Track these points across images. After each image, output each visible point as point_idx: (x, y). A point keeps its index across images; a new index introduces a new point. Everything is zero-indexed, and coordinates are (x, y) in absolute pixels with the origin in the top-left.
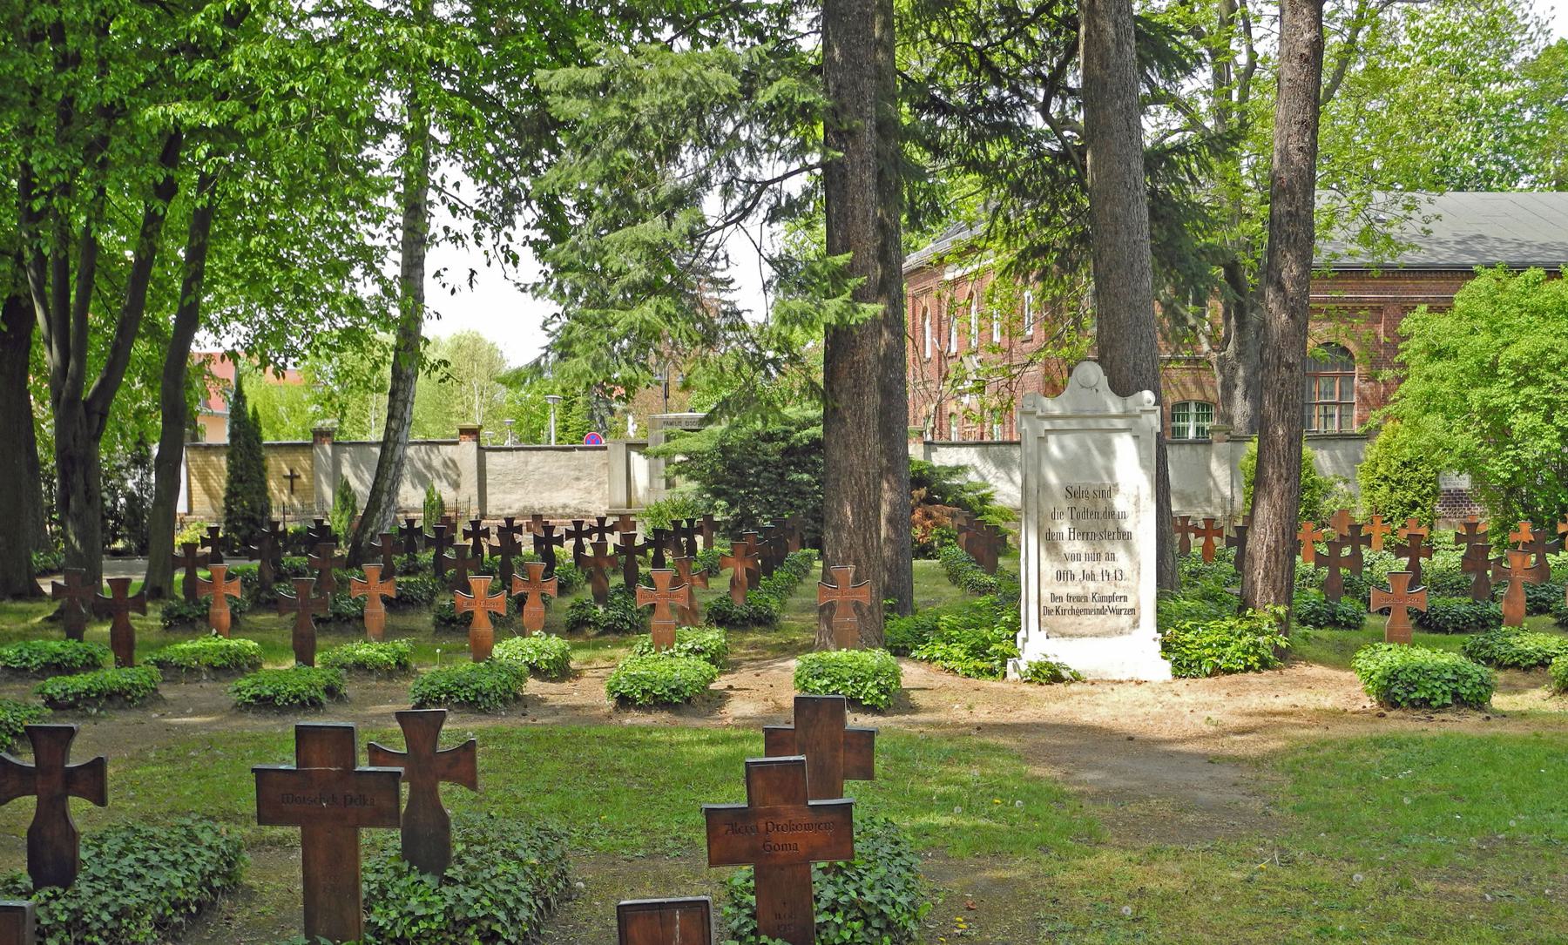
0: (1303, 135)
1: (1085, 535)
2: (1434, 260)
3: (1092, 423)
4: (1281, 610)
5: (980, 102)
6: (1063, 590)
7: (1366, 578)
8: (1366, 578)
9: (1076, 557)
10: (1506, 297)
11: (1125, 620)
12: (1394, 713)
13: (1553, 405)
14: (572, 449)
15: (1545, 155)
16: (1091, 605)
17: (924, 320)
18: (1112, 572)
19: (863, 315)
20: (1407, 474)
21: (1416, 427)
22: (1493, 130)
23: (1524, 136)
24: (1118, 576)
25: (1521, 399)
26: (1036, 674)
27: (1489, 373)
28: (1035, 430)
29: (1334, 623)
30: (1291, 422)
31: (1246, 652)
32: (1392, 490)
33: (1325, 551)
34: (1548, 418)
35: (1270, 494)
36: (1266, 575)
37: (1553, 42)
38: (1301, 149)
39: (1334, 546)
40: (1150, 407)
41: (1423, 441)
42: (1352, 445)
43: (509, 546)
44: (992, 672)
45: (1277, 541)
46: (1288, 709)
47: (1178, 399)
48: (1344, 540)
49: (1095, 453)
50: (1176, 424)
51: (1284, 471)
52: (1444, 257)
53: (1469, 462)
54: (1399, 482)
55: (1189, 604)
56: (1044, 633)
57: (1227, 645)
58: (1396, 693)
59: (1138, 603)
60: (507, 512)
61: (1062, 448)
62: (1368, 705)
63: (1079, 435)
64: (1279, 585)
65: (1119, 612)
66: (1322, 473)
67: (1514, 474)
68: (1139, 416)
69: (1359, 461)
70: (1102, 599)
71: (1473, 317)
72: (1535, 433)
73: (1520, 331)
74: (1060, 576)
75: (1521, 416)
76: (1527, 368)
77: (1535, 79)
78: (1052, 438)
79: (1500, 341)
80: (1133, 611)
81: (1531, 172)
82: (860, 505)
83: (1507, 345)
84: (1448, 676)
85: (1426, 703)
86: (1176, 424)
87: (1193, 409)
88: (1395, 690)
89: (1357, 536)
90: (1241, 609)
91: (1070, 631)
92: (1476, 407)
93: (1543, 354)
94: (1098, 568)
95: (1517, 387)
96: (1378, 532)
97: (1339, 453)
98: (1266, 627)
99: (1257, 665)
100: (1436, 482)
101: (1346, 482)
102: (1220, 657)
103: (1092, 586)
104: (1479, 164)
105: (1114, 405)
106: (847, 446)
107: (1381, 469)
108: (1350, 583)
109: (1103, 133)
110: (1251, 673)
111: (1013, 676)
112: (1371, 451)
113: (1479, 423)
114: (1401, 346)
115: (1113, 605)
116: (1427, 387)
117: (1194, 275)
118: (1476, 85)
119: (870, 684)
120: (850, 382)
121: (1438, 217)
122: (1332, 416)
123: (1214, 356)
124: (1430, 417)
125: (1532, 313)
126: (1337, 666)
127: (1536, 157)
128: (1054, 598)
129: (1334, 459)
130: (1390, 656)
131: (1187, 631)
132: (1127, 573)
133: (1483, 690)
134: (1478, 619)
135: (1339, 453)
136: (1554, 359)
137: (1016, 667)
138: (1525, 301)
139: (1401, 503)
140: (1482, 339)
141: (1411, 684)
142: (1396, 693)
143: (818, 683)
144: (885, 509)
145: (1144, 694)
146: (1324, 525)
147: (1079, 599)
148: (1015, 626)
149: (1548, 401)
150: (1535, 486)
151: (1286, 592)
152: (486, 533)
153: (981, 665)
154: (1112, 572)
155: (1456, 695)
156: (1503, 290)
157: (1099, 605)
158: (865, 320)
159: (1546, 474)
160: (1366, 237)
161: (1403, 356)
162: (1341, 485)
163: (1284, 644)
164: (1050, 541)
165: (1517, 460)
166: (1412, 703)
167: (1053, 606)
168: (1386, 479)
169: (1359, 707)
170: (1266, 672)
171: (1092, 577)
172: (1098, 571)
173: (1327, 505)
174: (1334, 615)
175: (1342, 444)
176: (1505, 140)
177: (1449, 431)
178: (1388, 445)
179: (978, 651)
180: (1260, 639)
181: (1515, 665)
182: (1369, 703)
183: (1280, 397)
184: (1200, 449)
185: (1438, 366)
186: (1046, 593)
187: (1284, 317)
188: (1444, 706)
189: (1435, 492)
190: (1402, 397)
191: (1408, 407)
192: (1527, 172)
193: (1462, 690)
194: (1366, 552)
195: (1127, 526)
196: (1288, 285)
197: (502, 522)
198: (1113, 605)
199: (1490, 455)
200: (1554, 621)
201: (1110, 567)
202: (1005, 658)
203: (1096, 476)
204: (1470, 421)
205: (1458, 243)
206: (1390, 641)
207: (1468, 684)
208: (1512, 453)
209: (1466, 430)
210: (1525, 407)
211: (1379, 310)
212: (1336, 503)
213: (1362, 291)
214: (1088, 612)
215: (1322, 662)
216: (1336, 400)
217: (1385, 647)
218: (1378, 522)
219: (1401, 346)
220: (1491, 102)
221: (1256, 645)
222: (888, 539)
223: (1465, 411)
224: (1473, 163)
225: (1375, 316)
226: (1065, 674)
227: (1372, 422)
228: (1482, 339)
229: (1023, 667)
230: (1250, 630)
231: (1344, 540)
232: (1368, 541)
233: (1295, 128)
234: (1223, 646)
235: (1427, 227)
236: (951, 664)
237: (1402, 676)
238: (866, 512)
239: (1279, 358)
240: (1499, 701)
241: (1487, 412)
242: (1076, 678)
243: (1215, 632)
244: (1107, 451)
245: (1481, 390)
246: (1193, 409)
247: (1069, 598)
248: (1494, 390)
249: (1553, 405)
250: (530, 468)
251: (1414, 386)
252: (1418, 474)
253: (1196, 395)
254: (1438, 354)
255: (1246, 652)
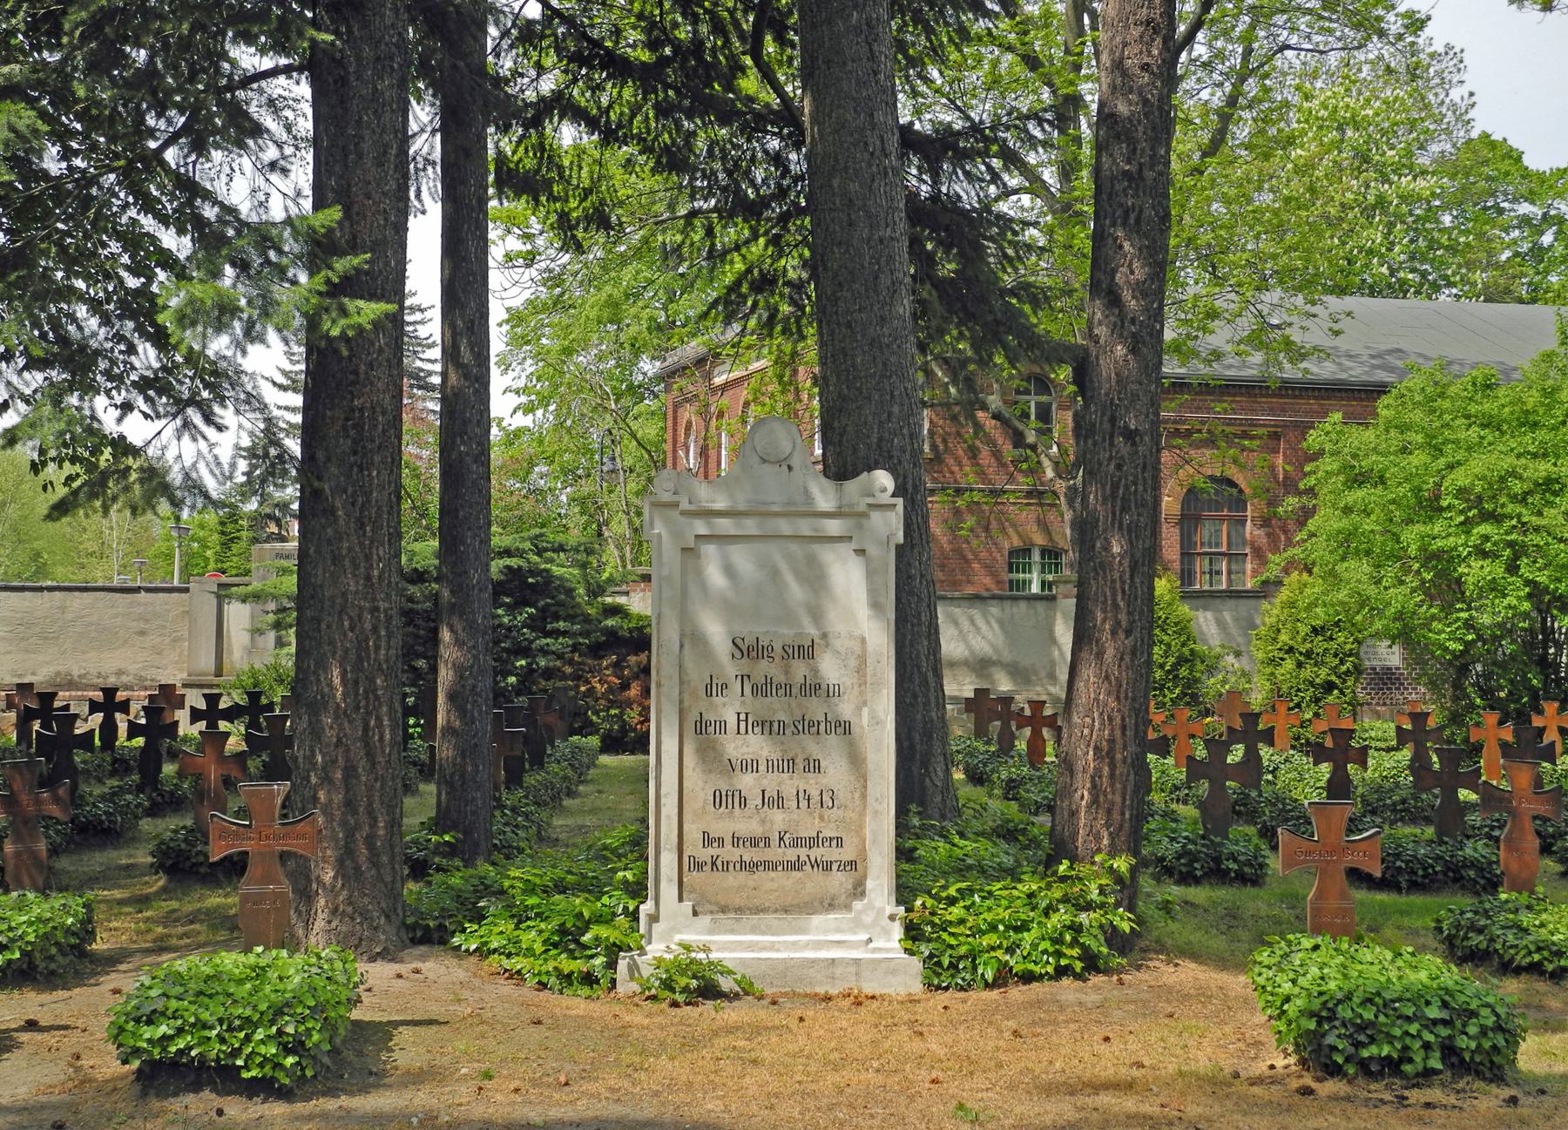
0: (1149, 44)
1: (766, 726)
2: (1343, 376)
3: (785, 527)
4: (1122, 864)
5: (668, 51)
6: (723, 826)
7: (1267, 791)
8: (1267, 791)
9: (750, 766)
10: (1447, 404)
11: (839, 881)
12: (1331, 1086)
13: (1518, 550)
14: (137, 590)
15: (1470, 265)
16: (776, 853)
17: (687, 435)
18: (815, 794)
19: (356, 319)
20: (1319, 644)
21: (1332, 576)
22: (1406, 231)
23: (1444, 240)
24: (827, 800)
25: (1473, 540)
26: (668, 985)
27: (1431, 507)
28: (677, 535)
29: (1218, 874)
30: (1132, 533)
31: (1057, 941)
32: (1300, 665)
33: (1201, 753)
34: (1512, 569)
35: (1100, 655)
36: (1095, 801)
37: (1475, 134)
38: (1145, 67)
39: (1218, 747)
40: (886, 498)
41: (1342, 595)
42: (1244, 605)
43: (157, 725)
44: (589, 979)
45: (1111, 741)
46: (1125, 1073)
47: (1017, 542)
48: (1234, 736)
49: (789, 578)
50: (1014, 576)
51: (1123, 617)
52: (1356, 373)
53: (1405, 634)
54: (1308, 654)
55: (969, 845)
56: (687, 905)
57: (1023, 927)
58: (1341, 1045)
59: (863, 852)
60: (112, 681)
61: (729, 570)
62: (1280, 1063)
63: (760, 546)
64: (1116, 816)
65: (827, 867)
66: (1205, 642)
67: (1468, 644)
68: (865, 515)
69: (1255, 627)
70: (797, 842)
71: (1404, 428)
72: (1496, 588)
73: (1469, 449)
74: (719, 799)
75: (1476, 564)
76: (1480, 498)
77: (1453, 177)
78: (710, 550)
79: (1442, 462)
80: (852, 864)
81: (1454, 285)
82: (358, 667)
83: (1451, 467)
84: (1433, 1012)
85: (1391, 1066)
86: (1014, 576)
87: (1036, 557)
88: (1331, 1039)
89: (1252, 731)
90: (1051, 861)
91: (738, 901)
92: (1413, 551)
93: (1502, 479)
94: (789, 784)
95: (1467, 525)
96: (1283, 726)
97: (1227, 616)
98: (1094, 895)
99: (1078, 966)
100: (1357, 655)
101: (1238, 654)
102: (1010, 951)
103: (778, 819)
104: (1392, 273)
105: (824, 496)
106: (336, 559)
107: (1284, 637)
108: (1244, 799)
109: (828, 63)
110: (1066, 981)
111: (625, 987)
112: (1271, 612)
113: (1418, 572)
114: (1307, 469)
115: (816, 853)
116: (1345, 523)
117: (998, 322)
118: (1386, 180)
119: (260, 1034)
120: (345, 444)
121: (1349, 314)
122: (1218, 573)
123: (1061, 486)
124: (1352, 563)
125: (1483, 426)
126: (1222, 962)
127: (1460, 266)
128: (708, 840)
129: (1221, 623)
130: (1318, 966)
131: (952, 901)
132: (841, 796)
133: (1500, 1041)
134: (1449, 867)
135: (1227, 616)
136: (1517, 487)
137: (633, 968)
138: (1473, 408)
139: (1312, 684)
140: (1418, 459)
141: (1361, 1028)
142: (1341, 1045)
143: (147, 1032)
144: (445, 676)
145: (858, 1029)
146: (1207, 713)
147: (754, 842)
148: (637, 890)
149: (1511, 544)
150: (1495, 663)
151: (1132, 838)
152: (124, 707)
153: (568, 965)
154: (815, 794)
155: (1448, 1049)
156: (1442, 395)
157: (791, 854)
158: (360, 329)
159: (1508, 647)
160: (1259, 338)
161: (1312, 481)
162: (1230, 659)
163: (1126, 927)
164: (702, 730)
165: (1469, 625)
166: (1363, 1065)
167: (705, 854)
168: (1291, 650)
169: (1260, 1068)
170: (1096, 980)
171: (779, 801)
172: (789, 791)
173: (1212, 685)
174: (1217, 860)
175: (1231, 603)
176: (1422, 243)
177: (1378, 582)
178: (1292, 604)
179: (567, 938)
180: (1083, 918)
181: (1535, 969)
182: (1284, 1062)
183: (1115, 487)
184: (1040, 607)
185: (1357, 495)
186: (693, 832)
187: (1120, 350)
188: (1428, 1073)
189: (1358, 670)
190: (1312, 535)
191: (1320, 550)
192: (1450, 284)
193: (1462, 1042)
194: (1265, 752)
195: (845, 709)
196: (1127, 295)
197: (98, 696)
198: (816, 853)
199: (1433, 618)
200: (1560, 868)
201: (812, 784)
202: (614, 951)
203: (788, 617)
204: (1407, 570)
205: (1373, 357)
206: (1316, 931)
207: (1473, 1030)
208: (1464, 615)
209: (1402, 582)
210: (1482, 554)
211: (1275, 436)
212: (1224, 682)
213: (1253, 411)
214: (770, 866)
215: (1195, 957)
216: (1224, 549)
217: (1307, 943)
218: (1282, 709)
219: (1307, 469)
220: (1403, 198)
221: (1077, 929)
222: (449, 730)
223: (1399, 556)
224: (1384, 270)
225: (1272, 443)
226: (726, 984)
227: (1272, 571)
228: (1418, 459)
229: (646, 971)
230: (1065, 900)
231: (1234, 736)
232: (1269, 737)
233: (1136, 32)
234: (1017, 929)
235: (1336, 327)
236: (518, 963)
237: (1344, 1012)
238: (372, 680)
239: (1113, 420)
240: (1535, 1054)
241: (1430, 557)
242: (746, 990)
243: (1003, 902)
244: (815, 578)
245: (1419, 528)
246: (1036, 557)
247: (736, 840)
248: (1437, 528)
249: (1518, 550)
250: (69, 616)
251: (1326, 521)
252: (1333, 645)
253: (1039, 539)
254: (1358, 479)
255: (1057, 941)
